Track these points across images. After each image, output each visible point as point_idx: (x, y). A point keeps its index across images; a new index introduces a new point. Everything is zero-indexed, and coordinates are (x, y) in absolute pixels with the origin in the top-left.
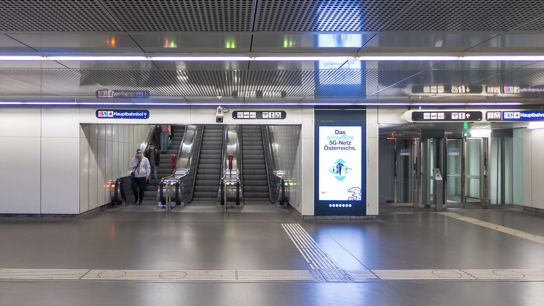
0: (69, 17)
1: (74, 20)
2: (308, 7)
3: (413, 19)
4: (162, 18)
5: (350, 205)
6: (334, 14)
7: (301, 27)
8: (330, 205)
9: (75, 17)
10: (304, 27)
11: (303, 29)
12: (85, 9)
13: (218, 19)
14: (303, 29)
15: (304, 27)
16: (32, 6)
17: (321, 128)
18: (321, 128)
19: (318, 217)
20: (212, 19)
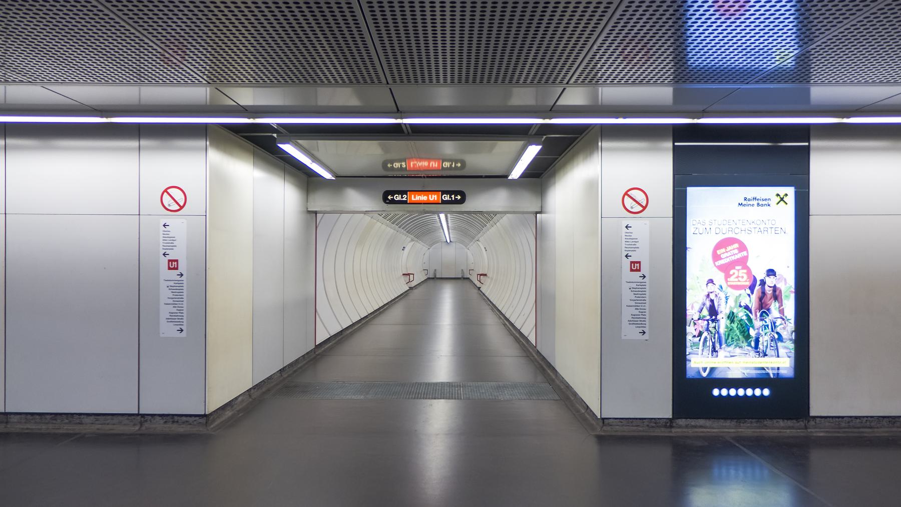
0: (201, 34)
1: (199, 40)
2: (545, 21)
3: (753, 40)
4: (412, 39)
5: (766, 392)
6: (615, 55)
7: (549, 78)
8: (716, 392)
9: (210, 34)
10: (560, 78)
11: (558, 80)
12: (221, 26)
13: (466, 42)
14: (558, 80)
15: (560, 78)
16: (156, 20)
17: (691, 191)
18: (691, 191)
19: (682, 422)
20: (484, 42)
